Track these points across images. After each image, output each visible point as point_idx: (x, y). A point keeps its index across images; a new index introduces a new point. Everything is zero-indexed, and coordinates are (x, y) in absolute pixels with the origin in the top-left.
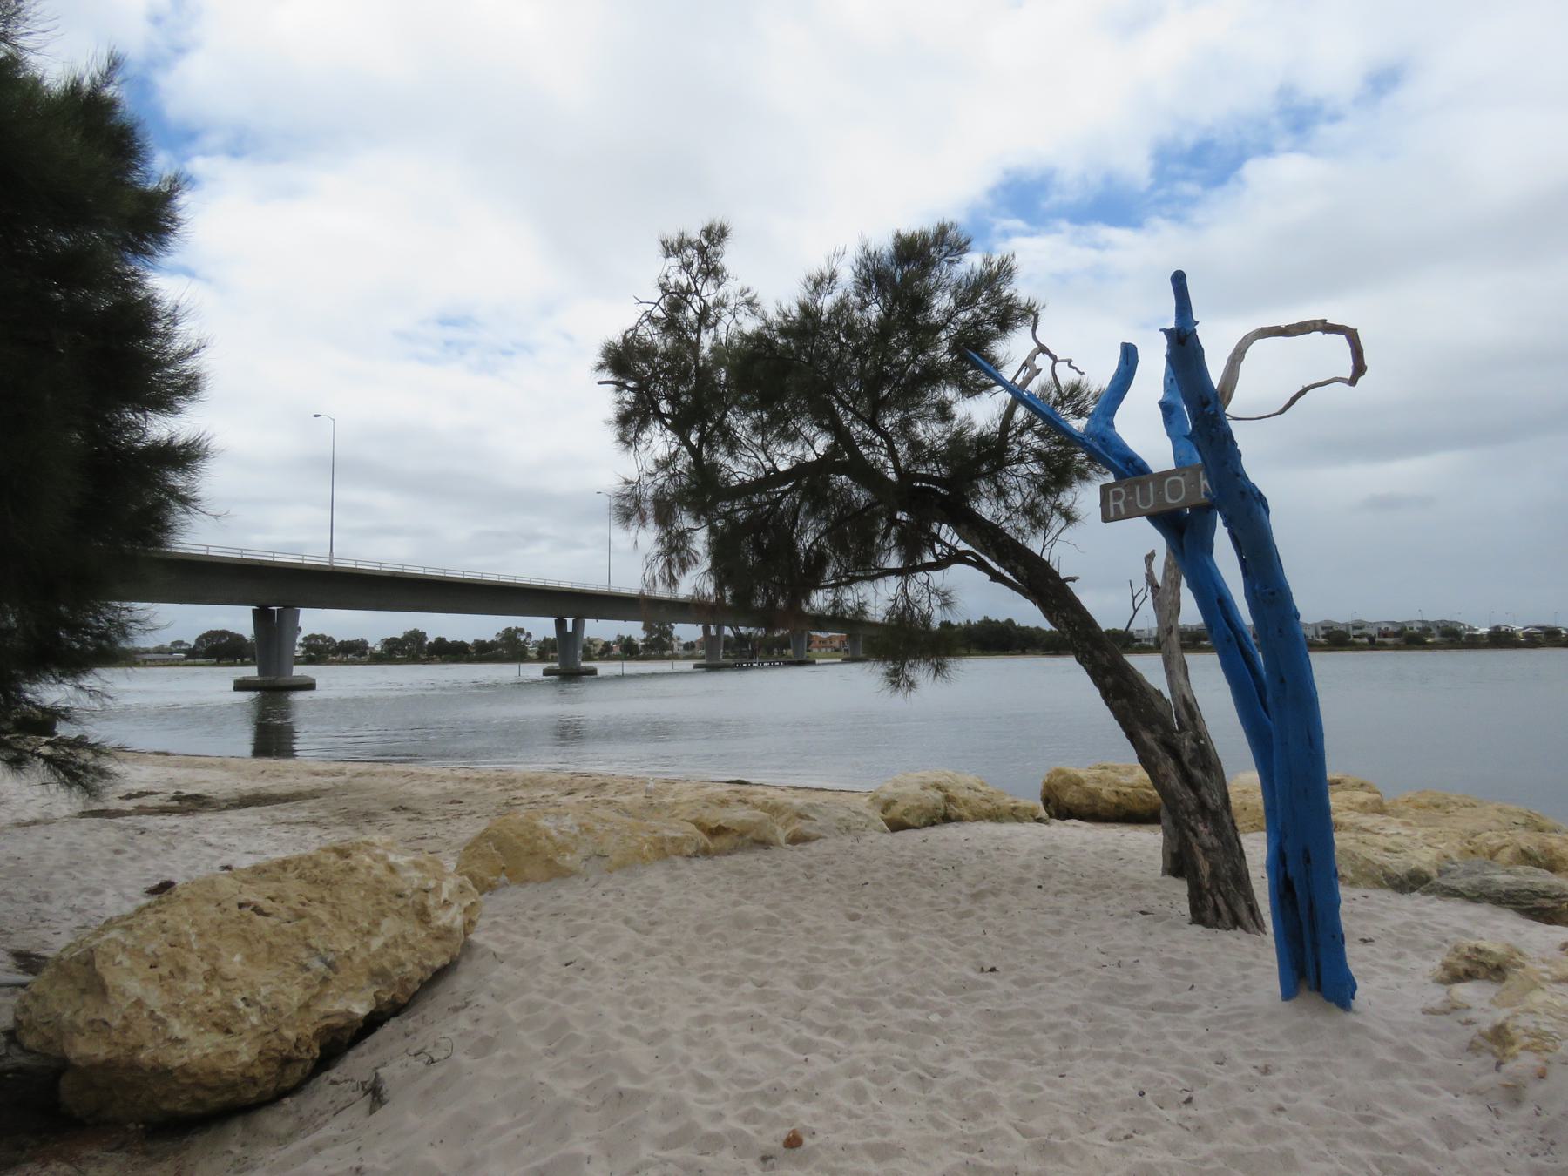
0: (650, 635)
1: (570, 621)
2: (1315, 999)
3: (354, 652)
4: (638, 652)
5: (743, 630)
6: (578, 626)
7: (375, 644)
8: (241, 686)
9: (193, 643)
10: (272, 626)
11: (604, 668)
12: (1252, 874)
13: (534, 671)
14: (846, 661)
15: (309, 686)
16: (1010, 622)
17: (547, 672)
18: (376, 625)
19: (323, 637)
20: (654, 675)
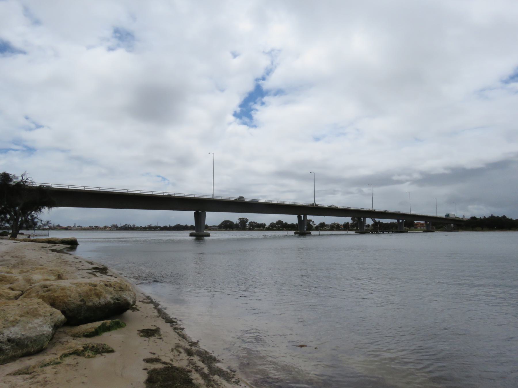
0: (354, 222)
1: (302, 216)
2: (119, 328)
3: (261, 227)
4: (349, 228)
5: (377, 220)
6: (305, 217)
7: (268, 224)
8: (191, 235)
9: (317, 224)
10: (199, 218)
11: (313, 233)
12: (78, 327)
13: (292, 233)
14: (425, 231)
15: (209, 235)
16: (242, 198)
17: (295, 233)
18: (329, 220)
19: (254, 222)
20: (331, 235)
